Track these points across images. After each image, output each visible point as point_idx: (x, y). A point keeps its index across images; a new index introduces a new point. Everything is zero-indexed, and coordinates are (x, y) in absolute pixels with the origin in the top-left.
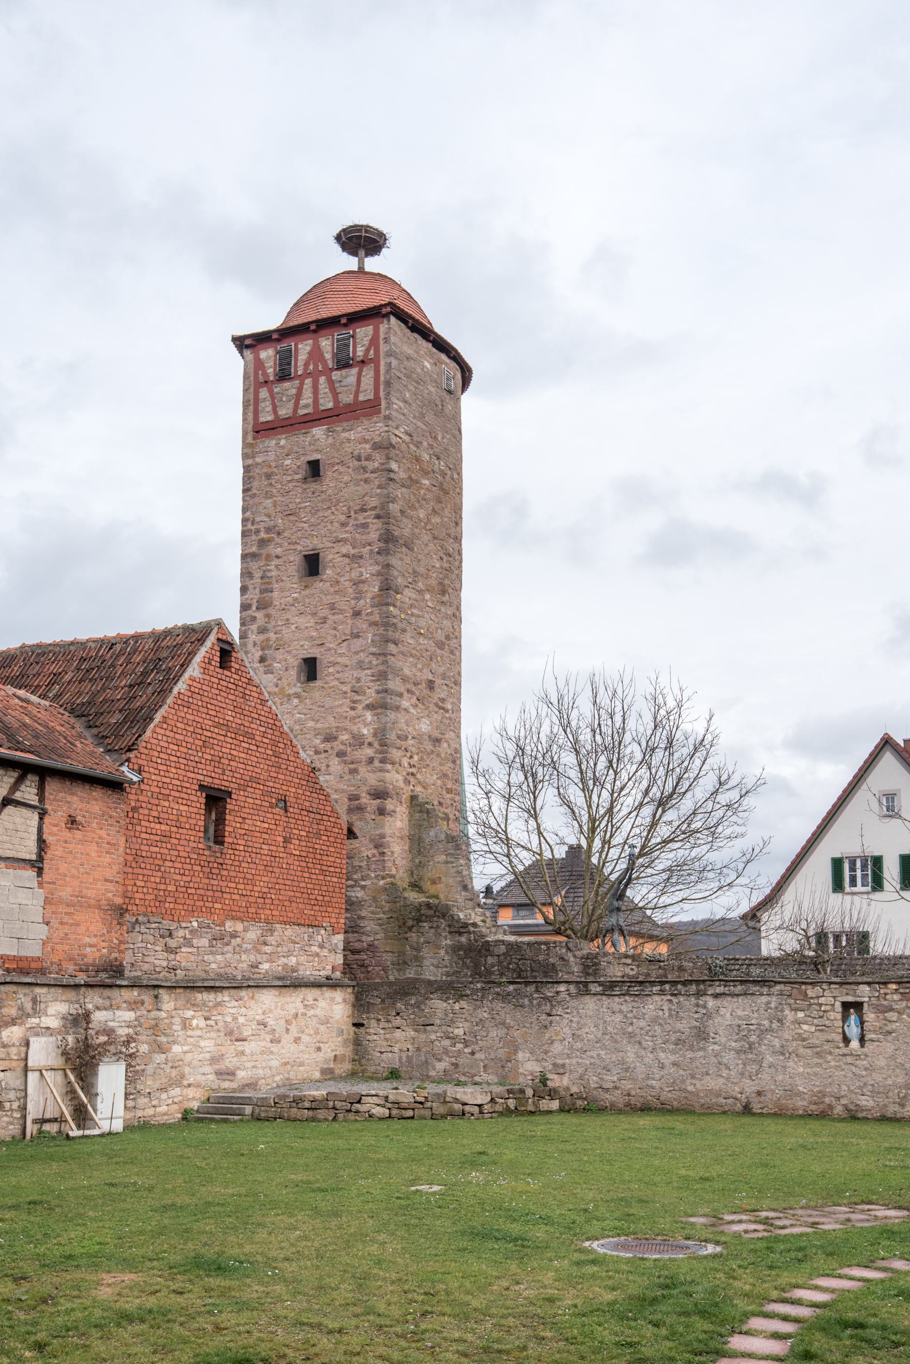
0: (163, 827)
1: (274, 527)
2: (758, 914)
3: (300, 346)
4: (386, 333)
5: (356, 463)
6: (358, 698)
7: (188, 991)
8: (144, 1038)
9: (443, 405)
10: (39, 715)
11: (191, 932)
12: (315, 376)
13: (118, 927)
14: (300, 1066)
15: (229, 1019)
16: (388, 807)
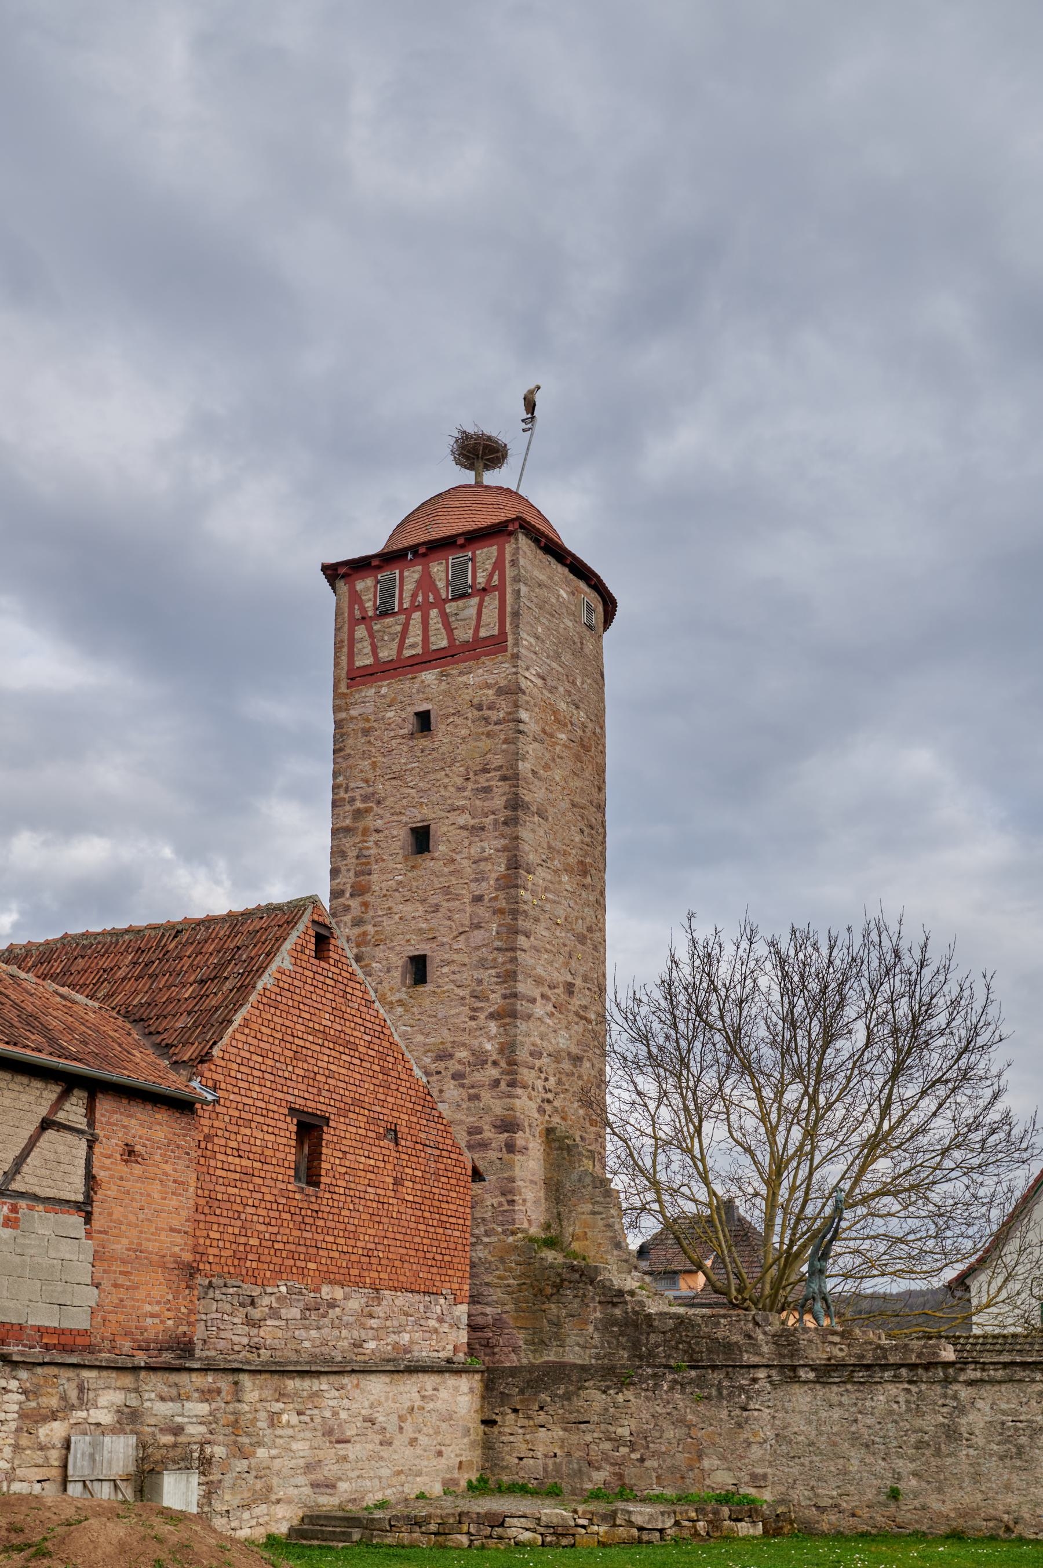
0: (245, 1162)
1: (373, 794)
2: (967, 1281)
3: (406, 574)
4: (514, 554)
5: (476, 713)
6: (480, 1005)
7: (276, 1377)
8: (221, 1438)
9: (582, 643)
10: (87, 1017)
11: (278, 1299)
12: (424, 609)
13: (187, 1291)
14: (416, 1476)
15: (328, 1414)
16: (518, 1142)
